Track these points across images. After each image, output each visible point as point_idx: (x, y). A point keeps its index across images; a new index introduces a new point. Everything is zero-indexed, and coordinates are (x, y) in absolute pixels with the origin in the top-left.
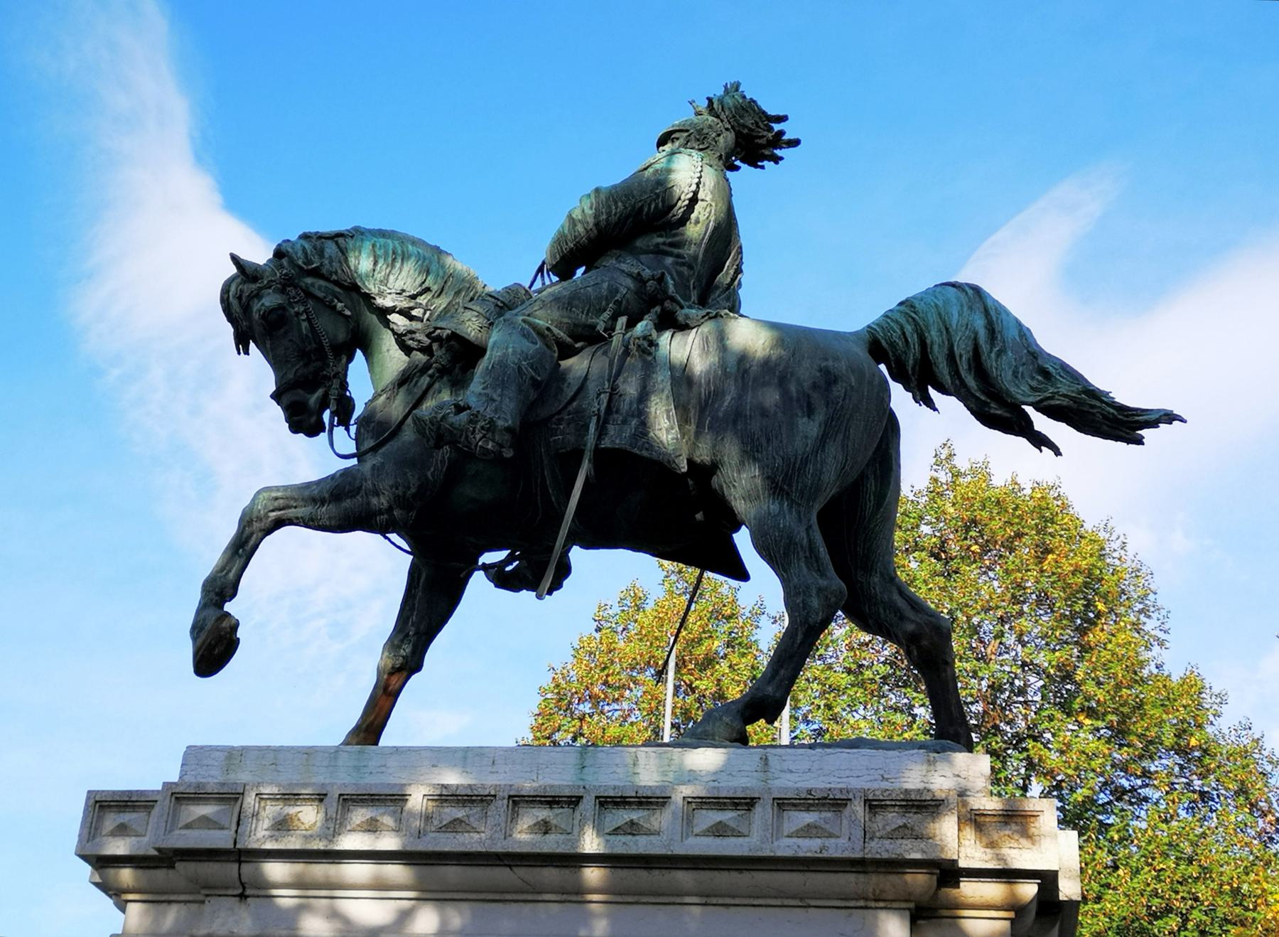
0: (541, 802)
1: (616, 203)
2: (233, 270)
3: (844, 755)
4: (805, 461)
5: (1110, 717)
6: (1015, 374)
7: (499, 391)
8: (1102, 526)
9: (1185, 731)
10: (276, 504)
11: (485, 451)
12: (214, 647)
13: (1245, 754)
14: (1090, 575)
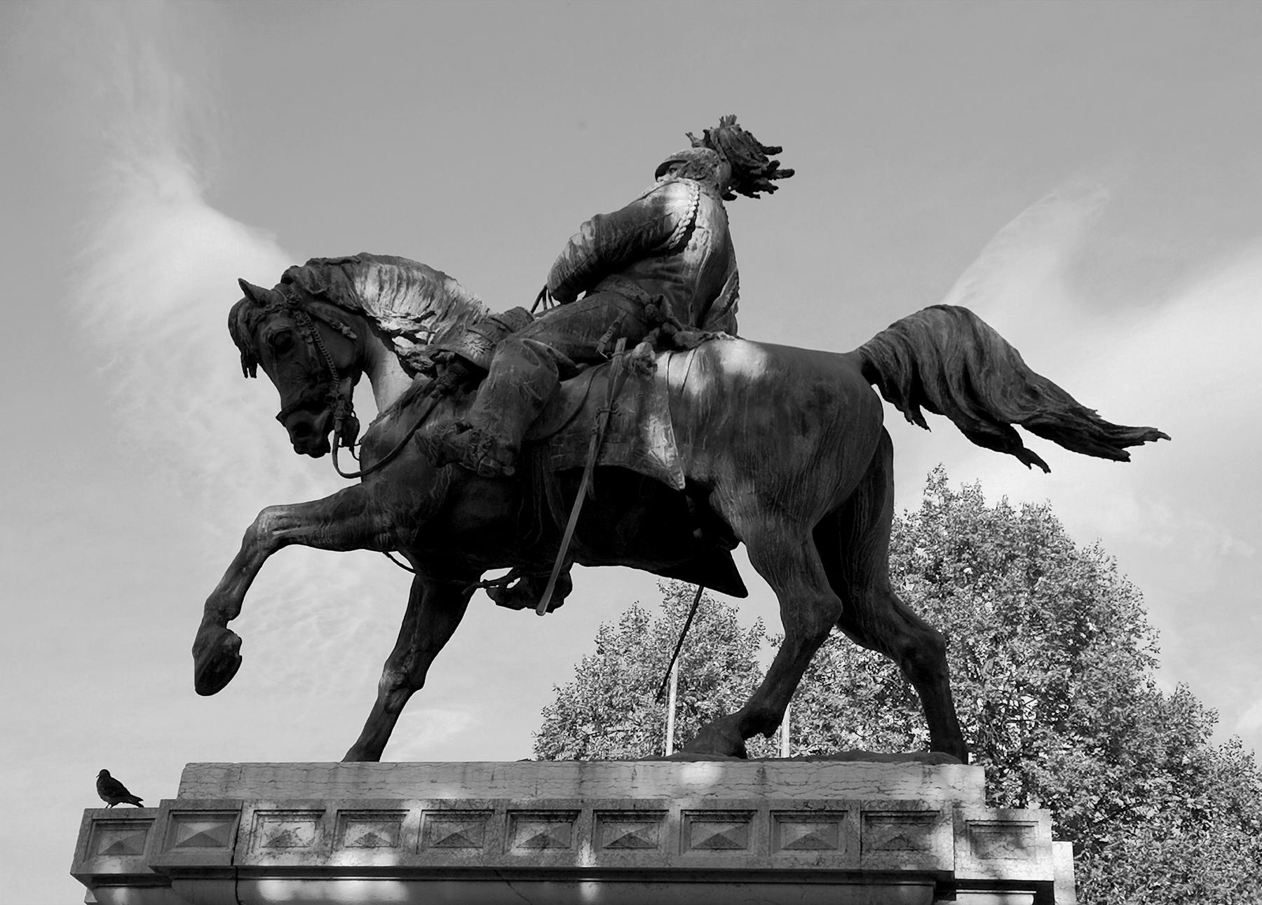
0: (539, 817)
1: (616, 230)
2: (241, 295)
3: (841, 768)
4: (800, 479)
5: (1101, 735)
6: (1004, 393)
7: (501, 410)
8: (1092, 548)
9: (1176, 749)
10: (280, 522)
11: (487, 469)
12: (216, 666)
13: (1236, 772)
14: (1081, 596)
